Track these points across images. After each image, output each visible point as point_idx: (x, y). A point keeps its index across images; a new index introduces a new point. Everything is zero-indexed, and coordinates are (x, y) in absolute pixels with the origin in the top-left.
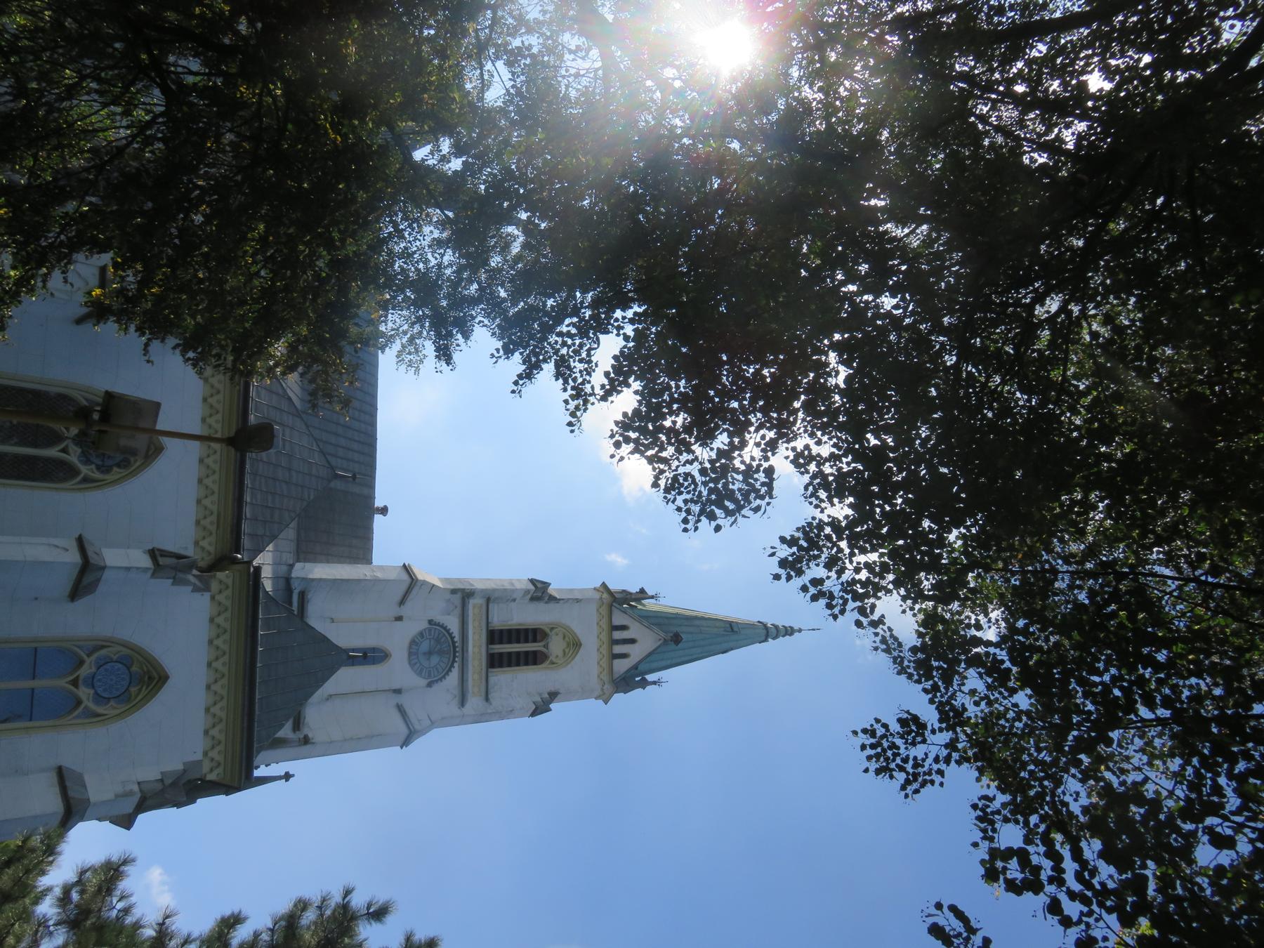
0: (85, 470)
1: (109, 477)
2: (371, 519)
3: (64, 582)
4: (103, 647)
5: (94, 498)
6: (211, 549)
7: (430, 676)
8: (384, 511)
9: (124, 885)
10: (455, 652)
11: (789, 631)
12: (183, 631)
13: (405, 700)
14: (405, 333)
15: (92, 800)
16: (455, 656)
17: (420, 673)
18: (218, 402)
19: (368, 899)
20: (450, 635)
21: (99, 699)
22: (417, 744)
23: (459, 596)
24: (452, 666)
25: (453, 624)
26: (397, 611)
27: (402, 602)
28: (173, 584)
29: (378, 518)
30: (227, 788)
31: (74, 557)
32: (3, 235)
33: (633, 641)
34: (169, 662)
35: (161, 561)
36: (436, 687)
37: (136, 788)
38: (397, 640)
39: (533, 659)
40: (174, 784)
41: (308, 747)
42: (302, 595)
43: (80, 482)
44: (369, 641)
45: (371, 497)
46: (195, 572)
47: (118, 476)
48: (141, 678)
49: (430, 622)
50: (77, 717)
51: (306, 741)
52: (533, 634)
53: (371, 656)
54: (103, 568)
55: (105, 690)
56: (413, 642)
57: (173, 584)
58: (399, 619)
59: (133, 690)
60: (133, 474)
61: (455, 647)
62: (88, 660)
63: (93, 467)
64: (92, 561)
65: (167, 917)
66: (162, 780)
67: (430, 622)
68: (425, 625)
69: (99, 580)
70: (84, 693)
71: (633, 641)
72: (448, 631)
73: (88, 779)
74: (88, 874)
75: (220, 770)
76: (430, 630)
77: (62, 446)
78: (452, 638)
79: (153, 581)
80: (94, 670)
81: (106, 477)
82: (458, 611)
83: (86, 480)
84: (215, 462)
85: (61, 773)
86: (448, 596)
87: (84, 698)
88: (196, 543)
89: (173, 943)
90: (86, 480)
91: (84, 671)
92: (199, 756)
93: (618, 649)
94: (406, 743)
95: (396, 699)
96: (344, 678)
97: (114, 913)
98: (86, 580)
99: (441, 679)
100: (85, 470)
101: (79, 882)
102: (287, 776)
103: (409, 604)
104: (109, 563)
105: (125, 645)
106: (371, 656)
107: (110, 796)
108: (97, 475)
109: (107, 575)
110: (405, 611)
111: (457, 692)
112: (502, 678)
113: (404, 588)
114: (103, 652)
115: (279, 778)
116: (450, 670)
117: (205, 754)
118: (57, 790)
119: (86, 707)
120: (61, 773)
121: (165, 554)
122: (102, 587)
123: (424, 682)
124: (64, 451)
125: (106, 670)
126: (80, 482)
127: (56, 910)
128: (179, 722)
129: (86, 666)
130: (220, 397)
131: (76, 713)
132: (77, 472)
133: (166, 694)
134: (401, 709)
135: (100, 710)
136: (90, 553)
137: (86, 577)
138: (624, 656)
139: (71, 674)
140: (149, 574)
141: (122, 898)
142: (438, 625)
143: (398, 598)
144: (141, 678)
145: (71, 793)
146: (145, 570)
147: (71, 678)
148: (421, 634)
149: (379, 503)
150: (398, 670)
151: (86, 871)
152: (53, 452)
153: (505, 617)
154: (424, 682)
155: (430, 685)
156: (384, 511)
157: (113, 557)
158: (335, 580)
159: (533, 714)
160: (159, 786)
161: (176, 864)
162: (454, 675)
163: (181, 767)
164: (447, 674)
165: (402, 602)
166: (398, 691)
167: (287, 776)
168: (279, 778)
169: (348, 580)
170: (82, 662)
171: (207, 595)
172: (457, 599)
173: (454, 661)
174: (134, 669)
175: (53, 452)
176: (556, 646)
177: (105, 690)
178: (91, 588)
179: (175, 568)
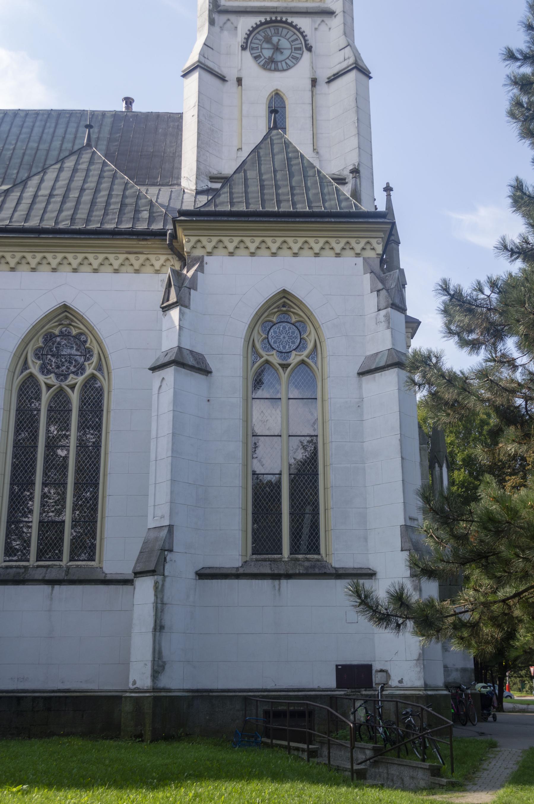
0: (89, 371)
1: (96, 350)
2: (137, 116)
3: (193, 381)
4: (254, 346)
5: (114, 360)
6: (163, 258)
7: (300, 49)
8: (129, 101)
9: (467, 289)
10: (276, 21)
12: (240, 278)
13: (323, 74)
15: (389, 346)
16: (281, 21)
17: (297, 59)
18: (13, 257)
19: (523, 29)
20: (258, 26)
21: (300, 347)
22: (368, 62)
23: (216, 16)
24: (291, 24)
25: (246, 24)
26: (232, 84)
27: (223, 79)
28: (196, 289)
29: (136, 108)
30: (391, 241)
31: (170, 373)
34: (270, 290)
35: (173, 298)
36: (311, 42)
37: (383, 313)
38: (262, 83)
40: (382, 281)
41: (362, 170)
42: (213, 179)
43: (102, 374)
44: (262, 110)
45: (116, 115)
46: (185, 272)
47: (94, 341)
48: (282, 310)
49: (244, 48)
50: (316, 363)
51: (355, 171)
53: (276, 109)
54: (180, 348)
55: (293, 342)
57: (196, 289)
58: (239, 81)
59: (294, 319)
60: (92, 330)
61: (271, 21)
62: (265, 357)
63: (86, 363)
64: (173, 358)
65: (505, 247)
66: (378, 291)
67: (244, 48)
68: (247, 54)
69: (191, 352)
70: (294, 359)
72: (254, 29)
73: (371, 351)
74: (453, 327)
75: (374, 241)
76: (252, 49)
77: (69, 390)
78: (262, 24)
79: (192, 306)
80: (274, 352)
81: (96, 352)
82: (233, 18)
83: (99, 368)
84: (75, 258)
85: (361, 374)
86: (217, 29)
87: (299, 359)
88: (157, 272)
89: (531, 239)
90: (99, 368)
91: (275, 359)
92: (360, 260)
94: (366, 73)
96: (297, 135)
97: (494, 296)
98: (191, 361)
99: (304, 37)
100: (89, 371)
101: (458, 334)
102: (388, 189)
103: (224, 71)
104: (175, 344)
105: (252, 328)
106: (276, 109)
107: (388, 332)
108: (95, 359)
109: (186, 345)
110: (231, 74)
111: (318, 20)
113: (208, 77)
114: (258, 346)
115: (389, 196)
116: (295, 27)
117: (358, 255)
118: (377, 375)
119: (308, 357)
120: (361, 374)
121: (167, 298)
122: (198, 349)
123: (306, 55)
124: (72, 387)
125: (275, 342)
126: (102, 374)
127: (482, 351)
128: (326, 279)
129: (270, 359)
130: (8, 256)
131: (312, 364)
132: (93, 377)
133: (299, 292)
134: (330, 81)
135: (310, 346)
136: (167, 359)
137: (189, 363)
139: (276, 370)
140: (186, 310)
141: (481, 290)
142: (247, 39)
143: (216, 82)
144: (282, 310)
145: (382, 364)
146: (181, 313)
147: (280, 369)
149: (122, 107)
150: (292, 82)
151: (449, 329)
152: (75, 397)
154: (306, 55)
155: (309, 49)
156: (129, 101)
157: (169, 342)
158: (198, 147)
160: (384, 293)
161: (454, 243)
163: (368, 276)
164: (299, 30)
165: (223, 79)
166: (314, 82)
167: (388, 189)
168: (389, 196)
169: (199, 134)
170: (267, 362)
171: (207, 259)
172: (220, 19)
173: (286, 22)
174: (275, 319)
175: (75, 397)
177: (293, 342)
178: (199, 358)
179: (179, 289)
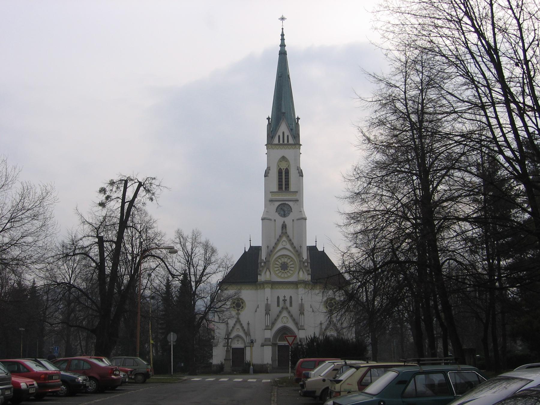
11: (283, 35)
14: (362, 292)
32: (539, 167)
33: (283, 133)
38: (280, 220)
39: (287, 172)
52: (280, 172)
53: (284, 226)
56: (281, 216)
71: (283, 133)
85: (297, 192)
93: (286, 142)
95: (295, 221)
112: (292, 188)
138: (288, 136)
148: (279, 214)
150: (288, 220)
153: (275, 188)
159: (302, 176)
162: (291, 204)
176: (284, 166)
